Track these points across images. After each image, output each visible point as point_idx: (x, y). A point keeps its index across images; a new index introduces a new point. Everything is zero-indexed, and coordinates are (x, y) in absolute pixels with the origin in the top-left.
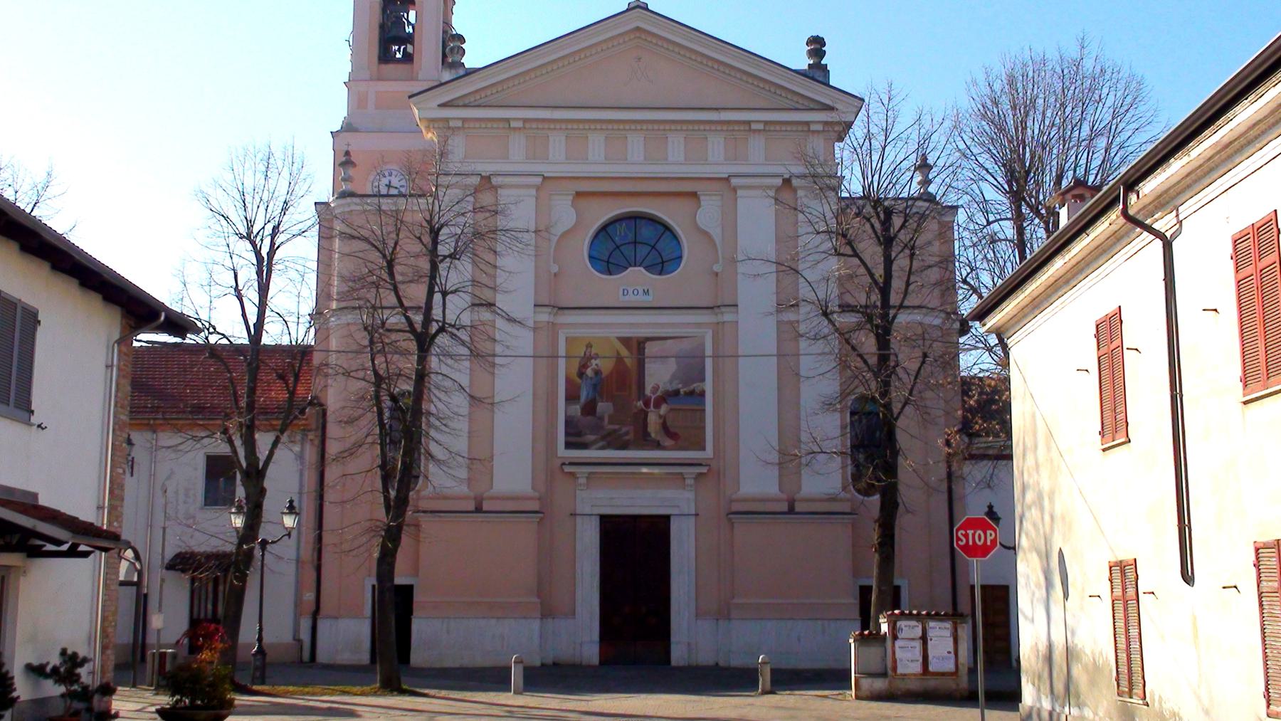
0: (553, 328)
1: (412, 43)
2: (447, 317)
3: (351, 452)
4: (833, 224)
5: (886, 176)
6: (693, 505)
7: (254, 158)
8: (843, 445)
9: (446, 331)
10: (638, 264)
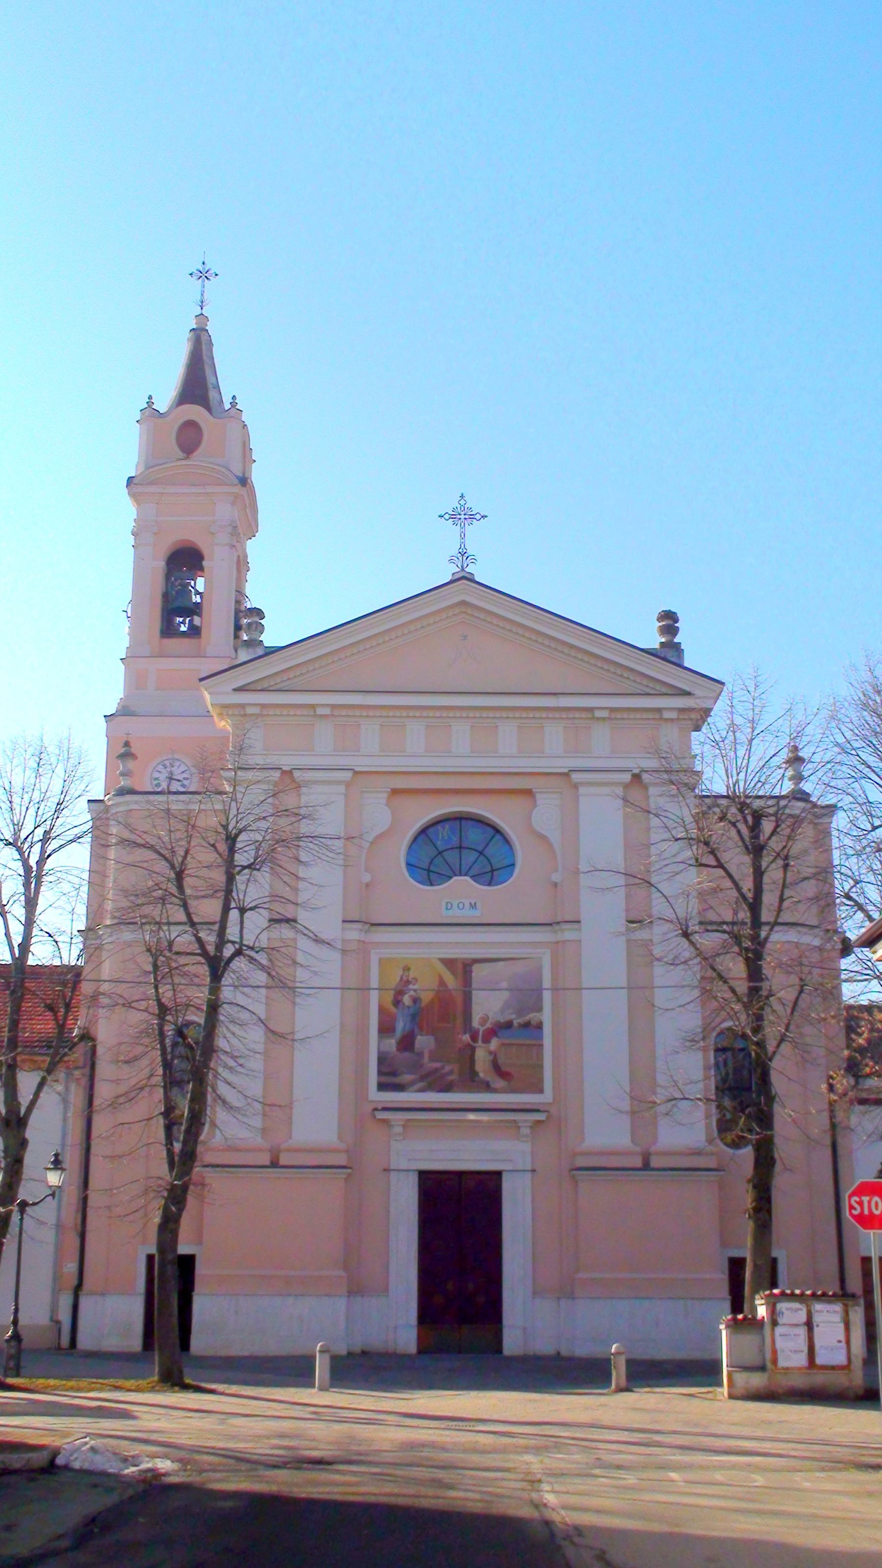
0: (364, 949)
1: (200, 615)
2: (245, 936)
3: (130, 1097)
4: (694, 833)
5: (753, 774)
6: (528, 1159)
7: (23, 752)
8: (706, 1089)
9: (244, 955)
10: (463, 871)
